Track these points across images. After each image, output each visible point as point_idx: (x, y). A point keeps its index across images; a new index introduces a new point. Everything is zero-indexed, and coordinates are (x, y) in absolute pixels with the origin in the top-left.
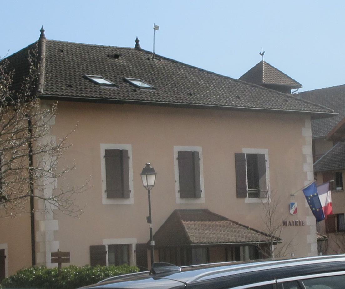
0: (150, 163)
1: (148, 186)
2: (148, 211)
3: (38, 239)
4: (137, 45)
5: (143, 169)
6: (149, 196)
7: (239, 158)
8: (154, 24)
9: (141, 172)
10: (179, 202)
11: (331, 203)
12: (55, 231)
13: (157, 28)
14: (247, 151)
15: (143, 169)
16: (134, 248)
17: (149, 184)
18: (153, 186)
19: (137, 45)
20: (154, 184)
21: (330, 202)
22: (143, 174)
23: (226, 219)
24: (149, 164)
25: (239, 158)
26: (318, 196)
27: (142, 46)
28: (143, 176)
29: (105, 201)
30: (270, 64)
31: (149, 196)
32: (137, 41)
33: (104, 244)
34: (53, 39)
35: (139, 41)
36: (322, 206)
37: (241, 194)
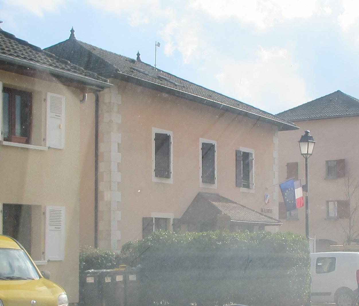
0: (309, 131)
1: (307, 154)
2: (308, 182)
3: (101, 207)
4: (138, 58)
5: (302, 136)
6: (306, 165)
7: (237, 152)
8: (156, 42)
9: (299, 140)
10: (200, 186)
11: (302, 197)
12: (118, 202)
13: (159, 45)
14: (243, 149)
15: (302, 136)
16: (172, 222)
17: (309, 153)
18: (311, 155)
19: (138, 58)
20: (313, 152)
21: (301, 196)
22: (301, 142)
23: (236, 203)
24: (308, 132)
25: (237, 152)
26: (294, 190)
27: (142, 59)
28: (301, 143)
29: (154, 179)
30: (216, 91)
31: (306, 165)
32: (138, 55)
33: (152, 217)
34: (81, 41)
35: (140, 55)
36: (296, 198)
37: (238, 185)
